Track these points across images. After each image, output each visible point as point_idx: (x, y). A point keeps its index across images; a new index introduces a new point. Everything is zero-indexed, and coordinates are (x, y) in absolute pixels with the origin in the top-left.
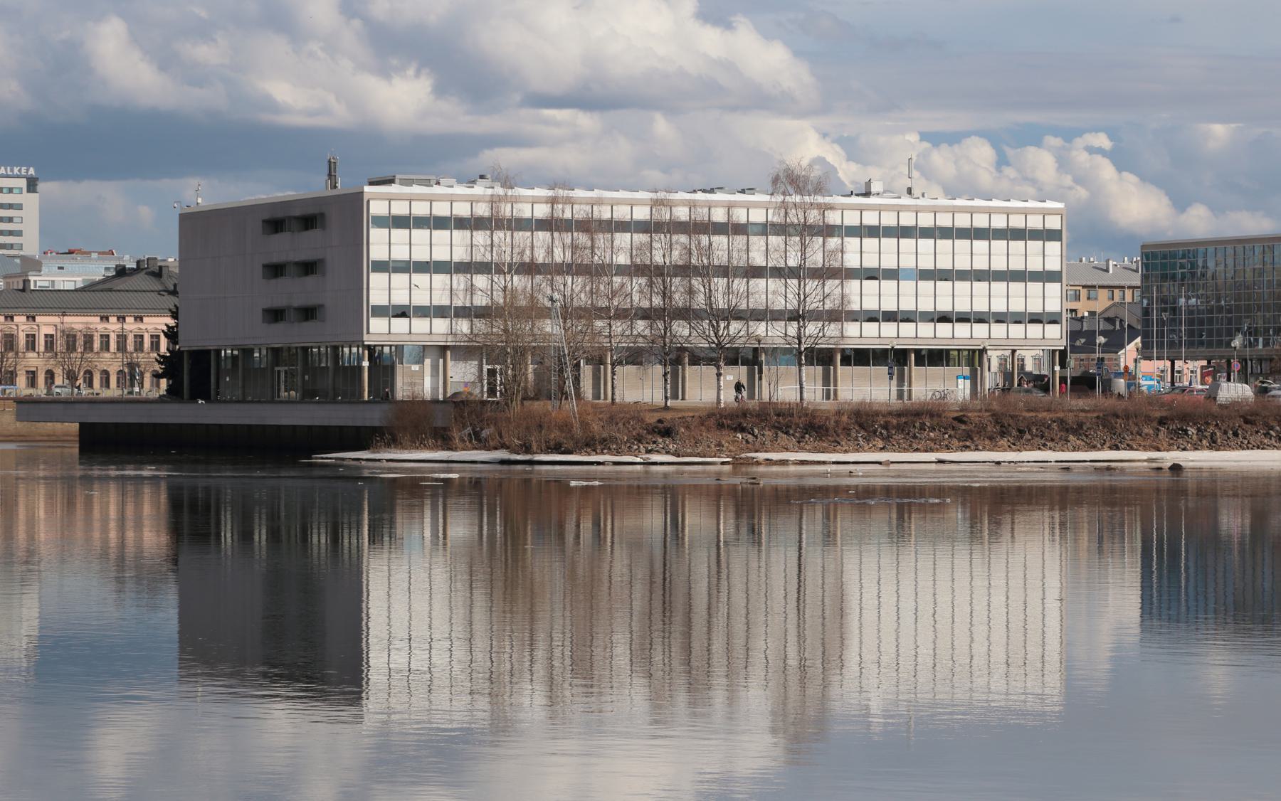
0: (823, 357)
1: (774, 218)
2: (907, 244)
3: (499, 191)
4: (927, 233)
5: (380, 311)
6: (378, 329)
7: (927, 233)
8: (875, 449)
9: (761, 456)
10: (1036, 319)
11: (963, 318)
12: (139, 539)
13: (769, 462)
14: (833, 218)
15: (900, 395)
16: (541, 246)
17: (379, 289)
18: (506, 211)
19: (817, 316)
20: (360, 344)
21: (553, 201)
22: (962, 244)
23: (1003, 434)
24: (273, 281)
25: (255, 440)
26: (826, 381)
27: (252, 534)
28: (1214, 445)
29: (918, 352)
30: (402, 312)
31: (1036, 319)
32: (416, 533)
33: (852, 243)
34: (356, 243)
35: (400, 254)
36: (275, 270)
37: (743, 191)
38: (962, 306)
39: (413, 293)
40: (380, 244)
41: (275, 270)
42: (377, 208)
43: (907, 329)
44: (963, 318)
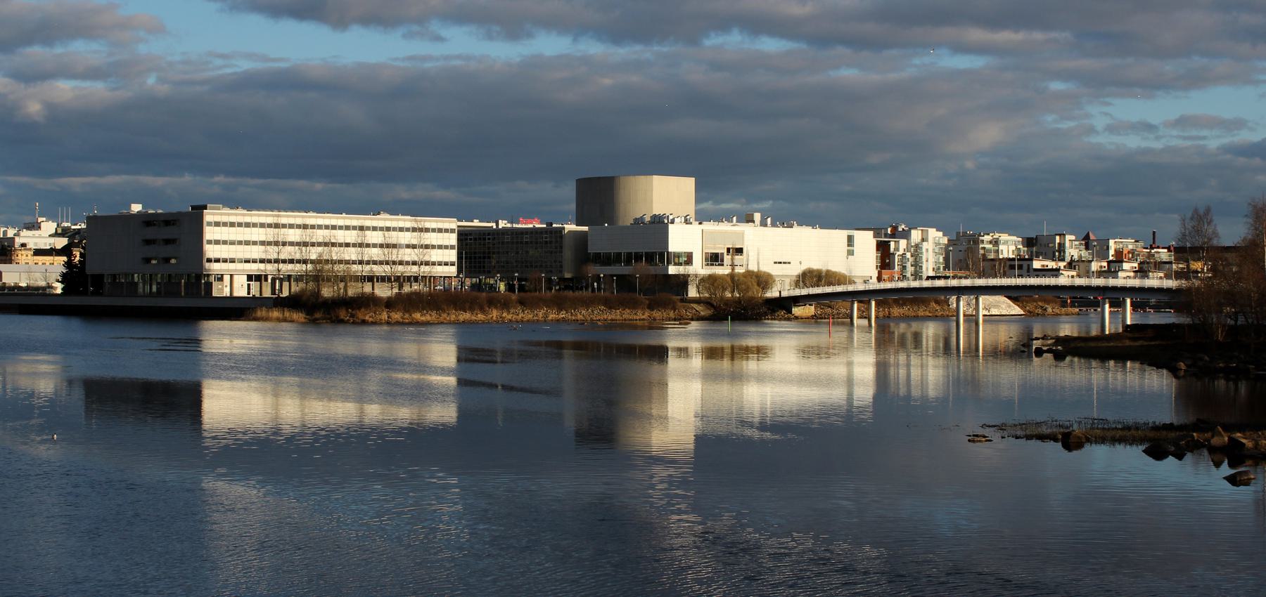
10: (446, 264)
36: (148, 242)
41: (148, 242)
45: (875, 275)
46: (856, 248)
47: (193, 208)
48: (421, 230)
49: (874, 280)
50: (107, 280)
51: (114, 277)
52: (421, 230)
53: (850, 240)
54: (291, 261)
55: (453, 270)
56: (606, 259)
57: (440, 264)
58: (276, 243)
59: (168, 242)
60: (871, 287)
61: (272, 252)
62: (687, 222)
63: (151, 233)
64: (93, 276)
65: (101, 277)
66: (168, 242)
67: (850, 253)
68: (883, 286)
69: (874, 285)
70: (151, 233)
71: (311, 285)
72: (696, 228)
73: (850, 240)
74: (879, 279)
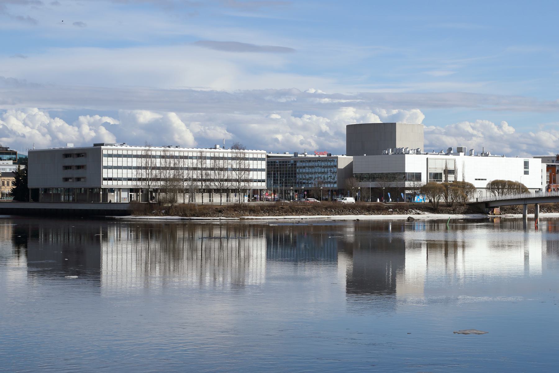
0: (209, 191)
1: (162, 154)
2: (120, 159)
3: (147, 148)
4: (125, 156)
5: (105, 179)
6: (105, 184)
7: (125, 156)
8: (266, 215)
9: (246, 217)
10: (259, 181)
11: (115, 179)
12: (189, 235)
13: (248, 219)
14: (247, 156)
15: (210, 201)
16: (158, 162)
17: (106, 173)
18: (149, 153)
19: (243, 181)
20: (100, 188)
21: (164, 151)
22: (125, 159)
23: (293, 211)
24: (66, 171)
25: (59, 210)
26: (210, 197)
27: (38, 235)
28: (339, 214)
29: (232, 189)
30: (110, 179)
31: (259, 181)
32: (112, 234)
33: (251, 162)
34: (99, 161)
35: (110, 164)
36: (67, 168)
37: (177, 147)
38: (115, 176)
39: (119, 174)
40: (106, 161)
41: (67, 168)
42: (105, 152)
43: (120, 183)
44: (115, 179)
45: (545, 185)
46: (530, 170)
47: (95, 145)
48: (146, 156)
49: (544, 190)
50: (42, 192)
51: (92, 189)
52: (146, 156)
53: (526, 164)
54: (130, 179)
55: (263, 185)
56: (361, 177)
57: (255, 181)
58: (146, 168)
59: (79, 167)
60: (544, 195)
61: (143, 174)
62: (418, 152)
63: (69, 162)
64: (32, 189)
65: (37, 190)
66: (79, 167)
67: (476, 179)
68: (549, 194)
69: (544, 193)
70: (69, 162)
71: (169, 196)
72: (422, 158)
73: (526, 164)
74: (548, 188)
